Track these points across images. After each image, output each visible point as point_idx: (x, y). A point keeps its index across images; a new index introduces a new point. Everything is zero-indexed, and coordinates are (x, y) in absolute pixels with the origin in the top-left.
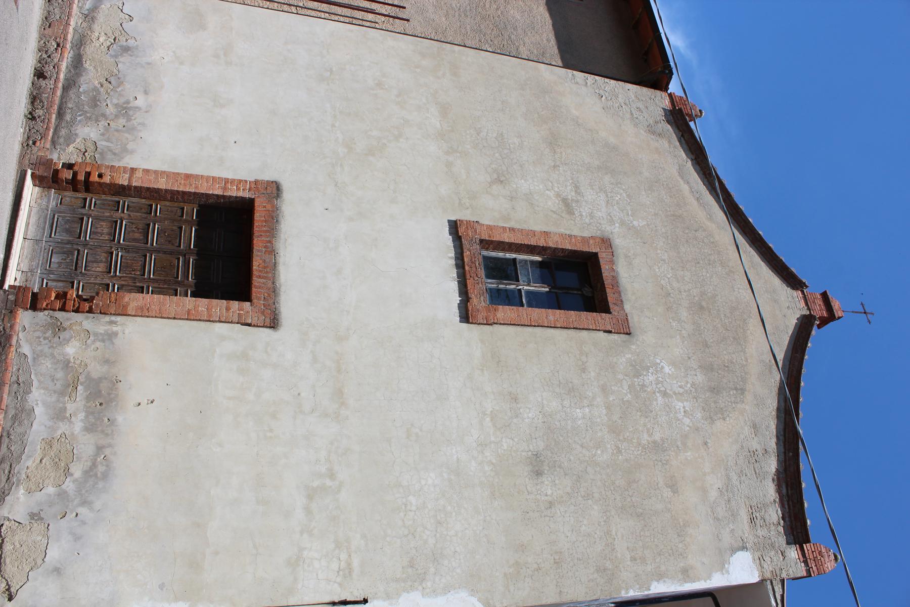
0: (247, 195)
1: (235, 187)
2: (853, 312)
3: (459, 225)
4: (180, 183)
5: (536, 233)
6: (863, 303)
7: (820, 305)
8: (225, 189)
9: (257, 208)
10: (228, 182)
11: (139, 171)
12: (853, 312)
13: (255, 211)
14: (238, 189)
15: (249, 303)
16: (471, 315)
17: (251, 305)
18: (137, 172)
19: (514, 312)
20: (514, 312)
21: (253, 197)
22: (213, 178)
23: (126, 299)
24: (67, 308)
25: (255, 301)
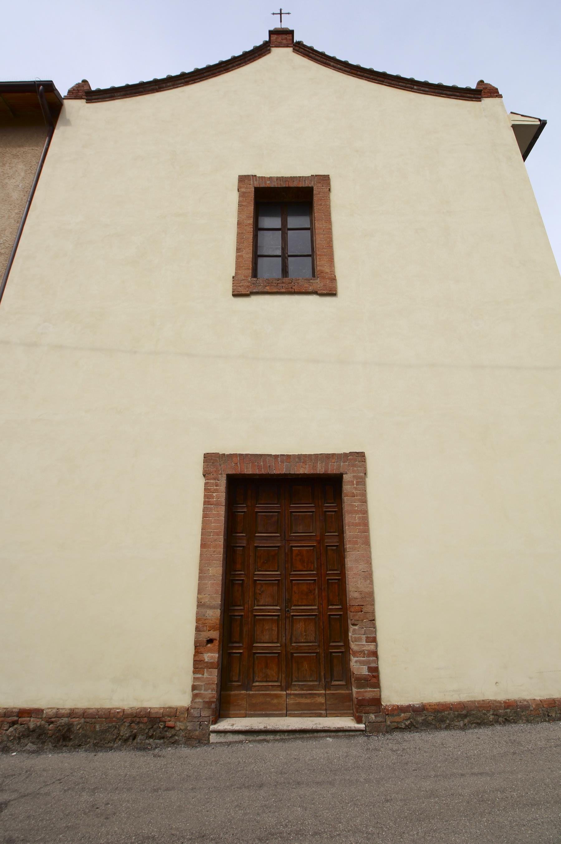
0: (223, 482)
1: (214, 494)
2: (281, 22)
3: (238, 293)
4: (214, 552)
5: (240, 232)
6: (487, 102)
7: (282, 39)
8: (217, 504)
9: (238, 471)
10: (208, 502)
11: (201, 598)
12: (281, 22)
13: (243, 473)
14: (216, 491)
15: (344, 476)
16: (330, 291)
17: (346, 474)
18: (203, 601)
19: (322, 258)
20: (322, 258)
21: (225, 476)
22: (205, 503)
23: (356, 595)
24: (272, 35)
25: (342, 471)
